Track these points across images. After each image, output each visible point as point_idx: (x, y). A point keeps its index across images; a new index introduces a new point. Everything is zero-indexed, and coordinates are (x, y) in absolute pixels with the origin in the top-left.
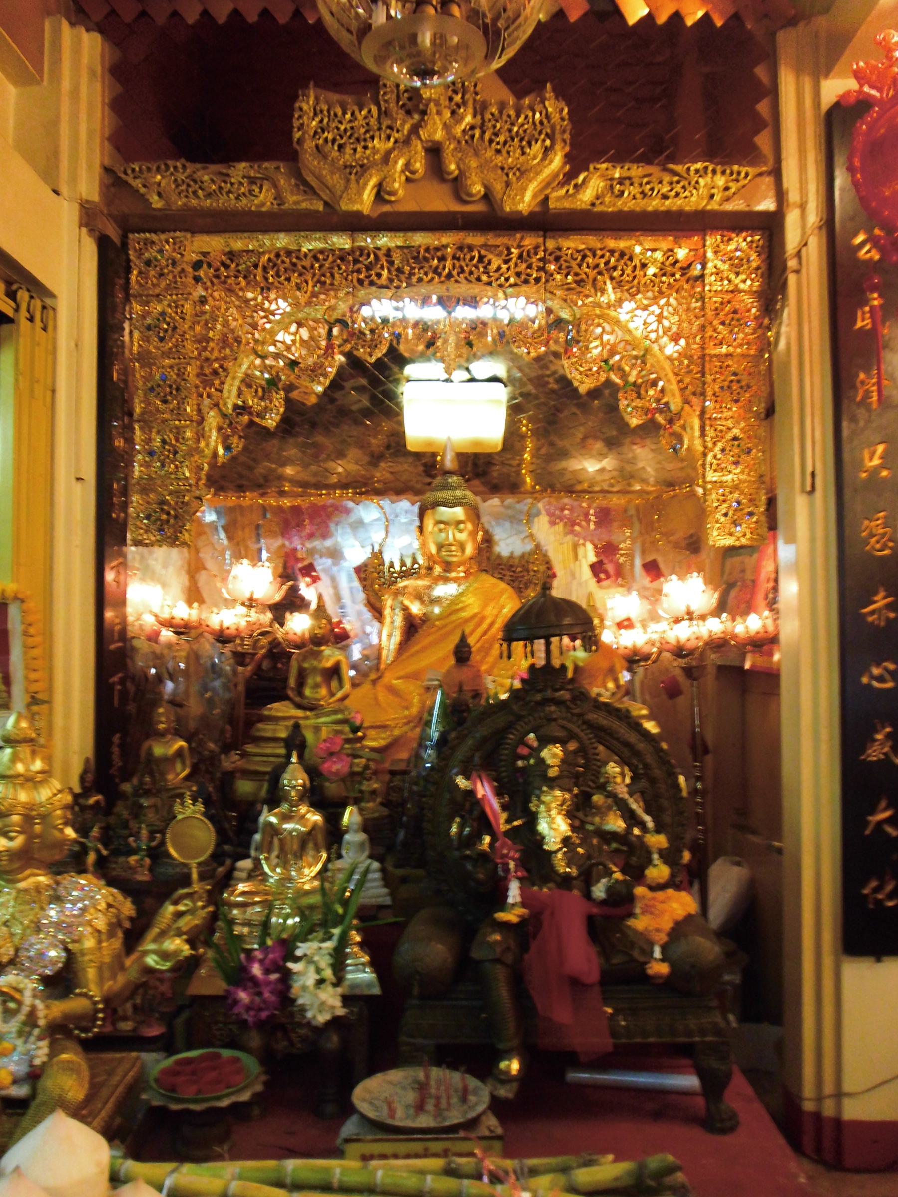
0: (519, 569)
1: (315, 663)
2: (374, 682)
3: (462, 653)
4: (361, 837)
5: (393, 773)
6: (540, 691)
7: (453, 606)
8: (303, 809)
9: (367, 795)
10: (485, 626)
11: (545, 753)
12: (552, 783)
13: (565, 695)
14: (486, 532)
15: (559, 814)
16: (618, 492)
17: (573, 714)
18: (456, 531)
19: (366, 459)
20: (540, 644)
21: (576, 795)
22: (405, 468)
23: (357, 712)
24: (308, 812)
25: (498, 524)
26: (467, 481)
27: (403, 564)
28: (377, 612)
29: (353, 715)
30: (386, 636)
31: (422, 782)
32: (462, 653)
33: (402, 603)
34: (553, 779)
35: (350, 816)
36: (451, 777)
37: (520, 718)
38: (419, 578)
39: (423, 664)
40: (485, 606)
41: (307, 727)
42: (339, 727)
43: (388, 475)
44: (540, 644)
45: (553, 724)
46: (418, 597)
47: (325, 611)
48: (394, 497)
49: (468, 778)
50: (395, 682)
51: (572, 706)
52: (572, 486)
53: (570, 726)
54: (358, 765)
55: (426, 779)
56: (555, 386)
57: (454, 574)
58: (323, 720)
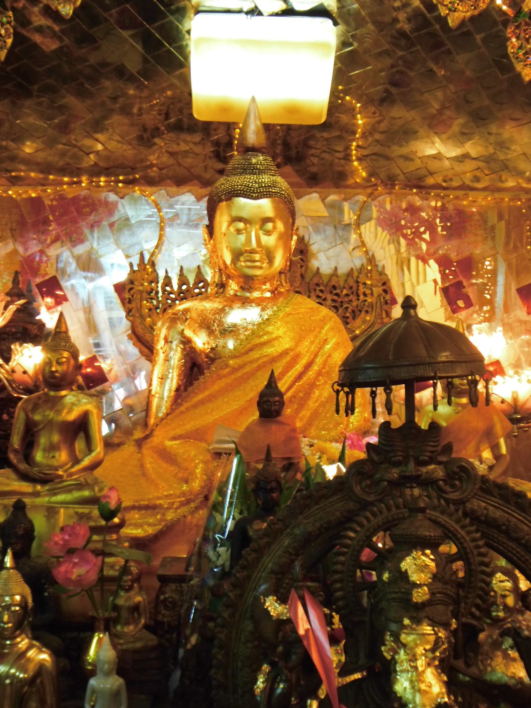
0: (345, 292)
1: (51, 414)
2: (139, 443)
3: (270, 404)
4: (115, 682)
5: (164, 580)
6: (397, 464)
7: (254, 339)
8: (23, 643)
9: (124, 614)
10: (299, 368)
11: (407, 564)
12: (418, 612)
13: (435, 470)
14: (301, 240)
15: (429, 665)
16: (485, 189)
17: (447, 501)
18: (261, 233)
19: (134, 133)
20: (400, 391)
21: (454, 633)
22: (187, 143)
23: (112, 489)
24: (30, 647)
25: (317, 230)
26: (278, 166)
27: (183, 280)
28: (146, 346)
29: (105, 491)
30: (161, 379)
31: (207, 595)
32: (270, 404)
33: (182, 333)
34: (422, 606)
35: (99, 649)
36: (257, 599)
37: (365, 505)
38: (207, 298)
39: (209, 419)
40: (299, 341)
41: (35, 507)
42: (84, 510)
43: (165, 159)
44: (400, 391)
45: (420, 516)
46: (206, 324)
47: (67, 339)
48: (174, 189)
49: (283, 600)
50: (168, 443)
51: (448, 488)
52: (421, 178)
53: (443, 519)
54: (112, 566)
55: (217, 594)
56: (407, 27)
57: (256, 294)
58: (61, 498)
